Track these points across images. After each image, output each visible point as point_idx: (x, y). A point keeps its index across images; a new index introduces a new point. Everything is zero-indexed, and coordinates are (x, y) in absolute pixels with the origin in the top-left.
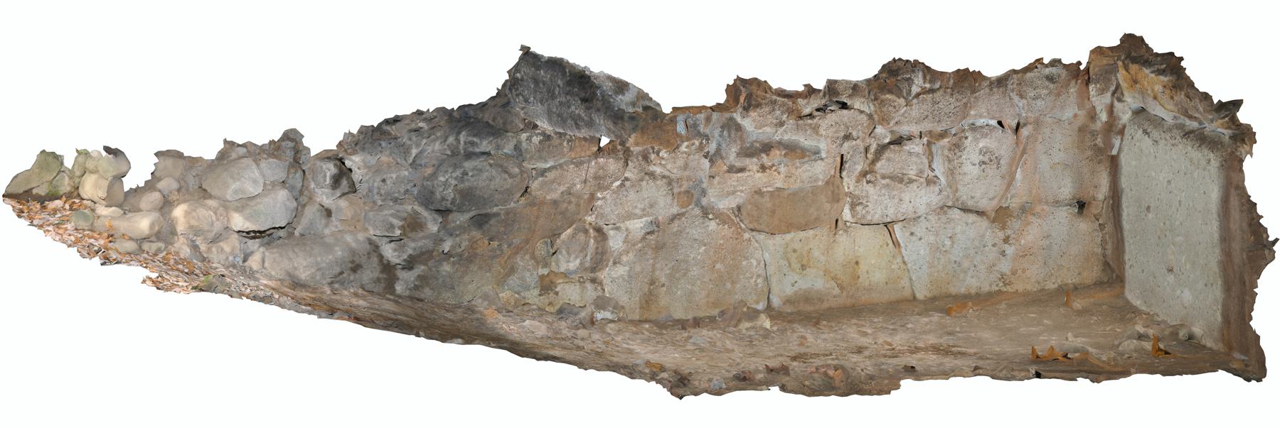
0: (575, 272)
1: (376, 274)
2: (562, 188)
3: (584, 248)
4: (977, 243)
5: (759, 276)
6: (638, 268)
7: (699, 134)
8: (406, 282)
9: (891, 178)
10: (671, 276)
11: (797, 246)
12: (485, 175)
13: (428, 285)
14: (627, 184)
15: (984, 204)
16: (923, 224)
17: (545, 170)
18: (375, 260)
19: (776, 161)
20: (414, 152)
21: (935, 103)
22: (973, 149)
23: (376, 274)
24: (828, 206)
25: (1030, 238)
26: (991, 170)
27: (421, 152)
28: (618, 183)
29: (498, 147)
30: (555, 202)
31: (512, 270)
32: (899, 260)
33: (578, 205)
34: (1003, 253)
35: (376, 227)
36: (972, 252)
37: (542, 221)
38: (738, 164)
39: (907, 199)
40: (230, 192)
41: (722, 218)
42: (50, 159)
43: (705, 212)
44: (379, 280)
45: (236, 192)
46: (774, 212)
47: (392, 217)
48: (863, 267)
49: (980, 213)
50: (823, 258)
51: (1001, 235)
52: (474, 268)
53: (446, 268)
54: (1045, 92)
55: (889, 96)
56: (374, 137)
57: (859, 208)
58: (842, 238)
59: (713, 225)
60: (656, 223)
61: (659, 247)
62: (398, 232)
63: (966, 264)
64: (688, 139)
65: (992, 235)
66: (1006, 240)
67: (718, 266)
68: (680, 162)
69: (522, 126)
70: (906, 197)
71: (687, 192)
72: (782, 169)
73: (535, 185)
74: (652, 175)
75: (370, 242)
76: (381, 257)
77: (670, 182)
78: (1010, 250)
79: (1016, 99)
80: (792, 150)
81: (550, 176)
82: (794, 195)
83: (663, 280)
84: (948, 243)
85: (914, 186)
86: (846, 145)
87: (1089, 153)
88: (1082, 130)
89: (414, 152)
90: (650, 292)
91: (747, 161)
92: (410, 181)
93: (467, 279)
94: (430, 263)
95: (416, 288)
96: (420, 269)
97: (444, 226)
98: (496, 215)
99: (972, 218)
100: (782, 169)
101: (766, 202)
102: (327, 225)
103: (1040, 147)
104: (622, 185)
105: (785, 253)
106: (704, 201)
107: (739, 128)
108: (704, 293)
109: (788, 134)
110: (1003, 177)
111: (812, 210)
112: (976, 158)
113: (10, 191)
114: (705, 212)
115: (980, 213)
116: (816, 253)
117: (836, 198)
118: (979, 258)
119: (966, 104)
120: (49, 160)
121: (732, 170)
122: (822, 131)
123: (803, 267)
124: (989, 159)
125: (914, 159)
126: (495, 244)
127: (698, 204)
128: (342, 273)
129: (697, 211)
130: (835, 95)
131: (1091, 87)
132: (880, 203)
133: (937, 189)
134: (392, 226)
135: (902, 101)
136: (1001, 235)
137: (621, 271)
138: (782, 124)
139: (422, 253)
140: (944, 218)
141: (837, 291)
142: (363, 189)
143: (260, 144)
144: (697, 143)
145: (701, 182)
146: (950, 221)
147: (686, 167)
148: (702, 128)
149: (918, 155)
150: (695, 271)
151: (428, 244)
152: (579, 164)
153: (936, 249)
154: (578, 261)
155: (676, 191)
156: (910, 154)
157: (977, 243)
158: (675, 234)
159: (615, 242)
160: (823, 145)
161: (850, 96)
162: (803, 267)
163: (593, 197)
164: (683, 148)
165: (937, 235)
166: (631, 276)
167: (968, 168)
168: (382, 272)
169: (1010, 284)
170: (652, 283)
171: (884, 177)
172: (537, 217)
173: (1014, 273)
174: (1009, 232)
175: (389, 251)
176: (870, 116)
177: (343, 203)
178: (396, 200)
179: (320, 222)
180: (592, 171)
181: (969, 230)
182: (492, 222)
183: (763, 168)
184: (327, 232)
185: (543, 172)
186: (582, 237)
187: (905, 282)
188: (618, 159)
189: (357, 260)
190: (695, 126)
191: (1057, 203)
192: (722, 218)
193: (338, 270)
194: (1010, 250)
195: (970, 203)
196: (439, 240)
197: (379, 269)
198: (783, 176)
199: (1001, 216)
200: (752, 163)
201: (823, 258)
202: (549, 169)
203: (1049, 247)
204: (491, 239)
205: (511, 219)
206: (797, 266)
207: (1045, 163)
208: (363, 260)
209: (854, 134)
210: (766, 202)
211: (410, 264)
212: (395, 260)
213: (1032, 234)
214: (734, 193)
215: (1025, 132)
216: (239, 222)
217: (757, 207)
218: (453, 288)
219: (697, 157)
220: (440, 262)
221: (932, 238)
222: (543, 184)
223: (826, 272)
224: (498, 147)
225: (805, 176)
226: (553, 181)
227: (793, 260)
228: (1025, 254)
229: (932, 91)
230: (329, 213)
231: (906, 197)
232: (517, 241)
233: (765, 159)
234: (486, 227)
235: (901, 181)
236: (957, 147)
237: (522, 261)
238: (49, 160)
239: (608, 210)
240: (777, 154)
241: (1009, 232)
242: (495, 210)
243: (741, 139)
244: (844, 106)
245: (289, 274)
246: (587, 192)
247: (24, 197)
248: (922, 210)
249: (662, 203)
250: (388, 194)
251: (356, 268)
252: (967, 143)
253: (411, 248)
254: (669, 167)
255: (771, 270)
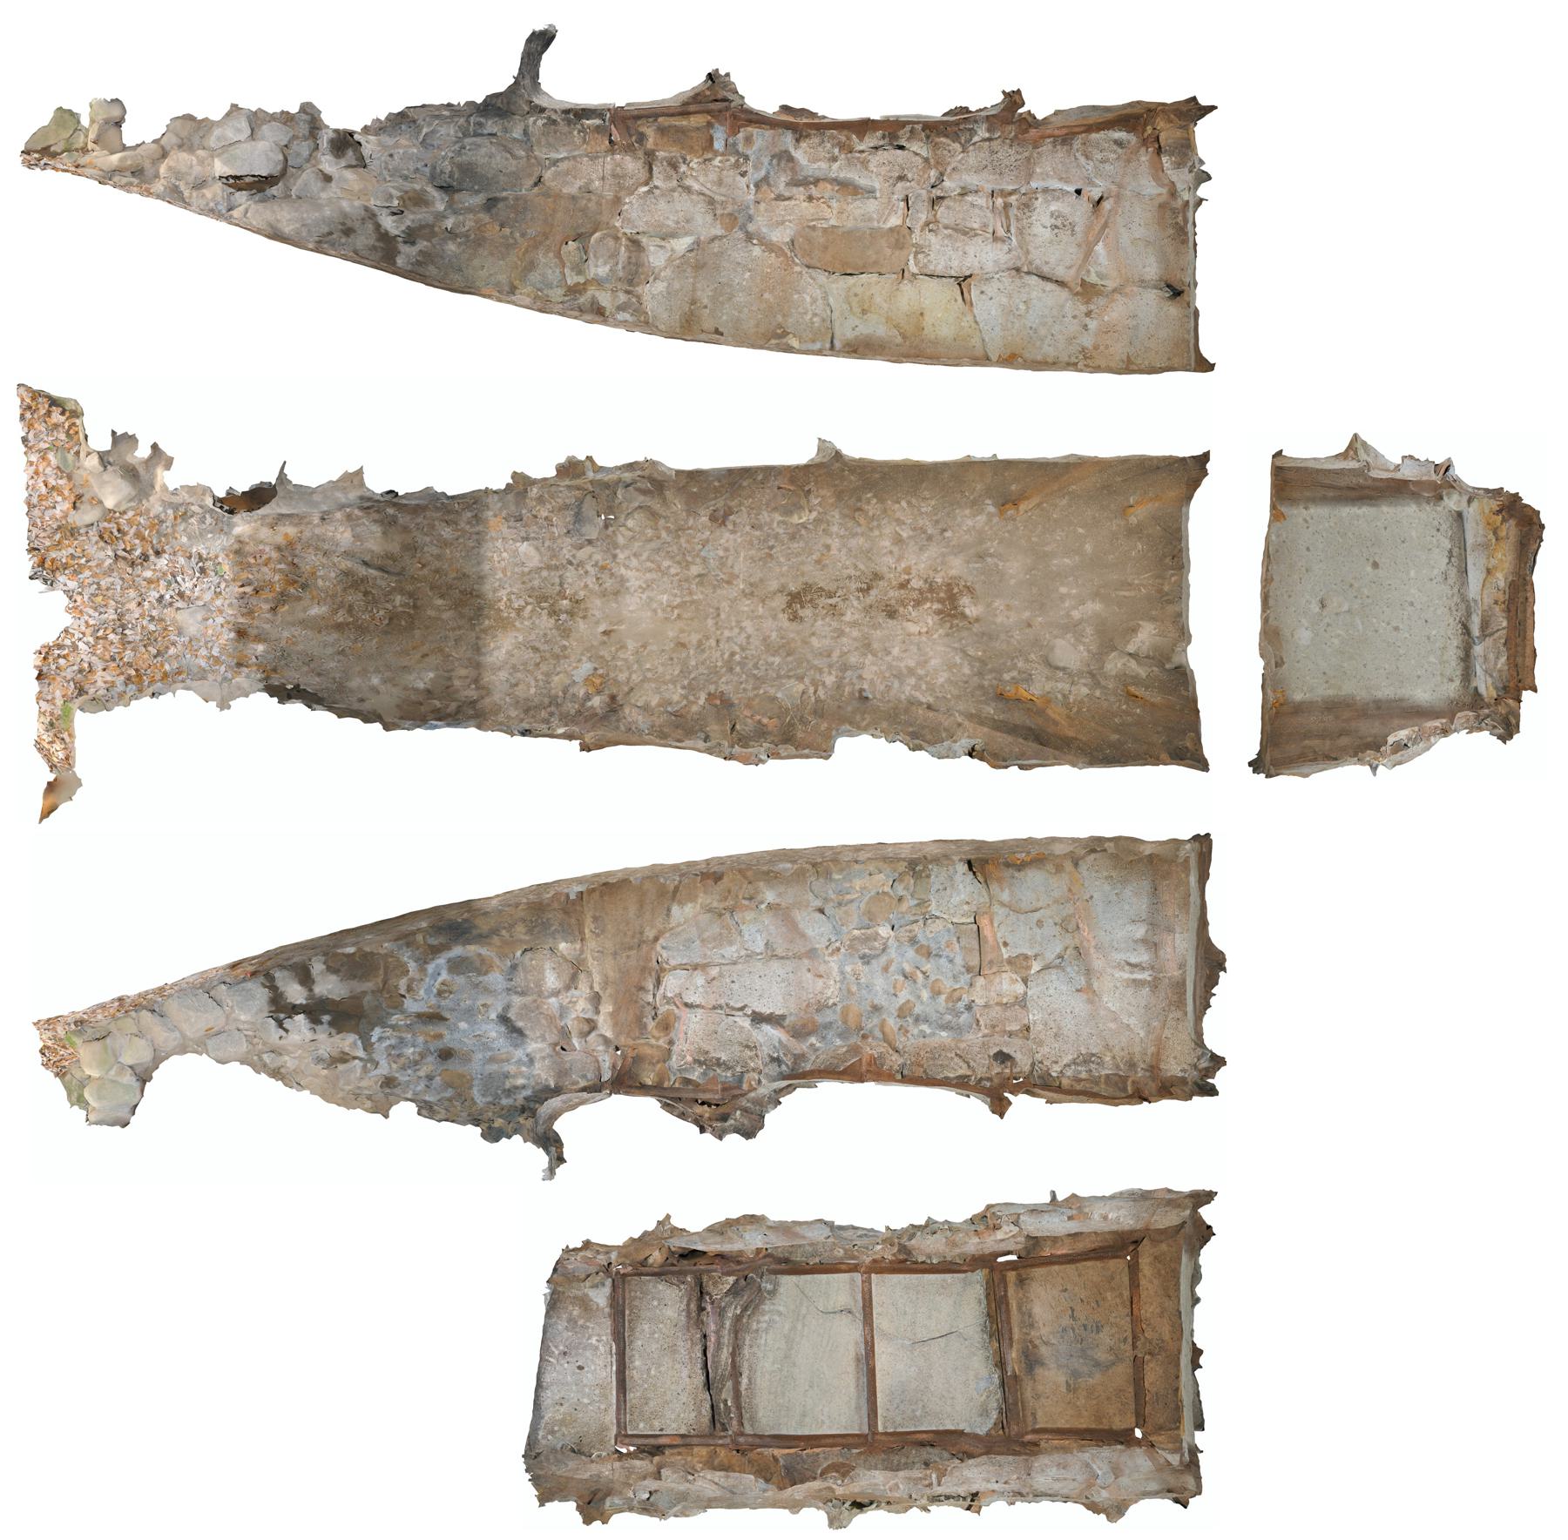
0: (607, 280)
1: (372, 242)
2: (579, 183)
3: (614, 255)
4: (1055, 312)
5: (815, 315)
6: (677, 286)
7: (737, 153)
8: (408, 256)
9: (955, 230)
10: (714, 299)
11: (859, 290)
12: (483, 151)
13: (433, 262)
14: (657, 192)
15: (1060, 272)
16: (995, 285)
17: (558, 160)
18: (370, 226)
19: (827, 195)
20: (425, 130)
21: (993, 152)
22: (1043, 214)
23: (372, 242)
24: (888, 251)
25: (1114, 315)
26: (1065, 236)
27: (433, 132)
28: (645, 189)
29: (506, 130)
30: (573, 198)
31: (532, 266)
32: (970, 318)
33: (599, 204)
34: (1085, 327)
35: (377, 198)
36: (1050, 320)
37: (560, 215)
38: (787, 194)
39: (972, 253)
40: (213, 138)
41: (770, 247)
42: (67, 116)
43: (749, 237)
44: (374, 248)
45: (218, 139)
46: (826, 248)
47: (394, 188)
48: (928, 321)
49: (1060, 283)
50: (885, 305)
51: (1083, 308)
52: (484, 252)
53: (451, 247)
54: (1113, 156)
55: (943, 140)
56: (403, 120)
57: (920, 256)
58: (906, 287)
59: (757, 251)
60: (698, 243)
61: (699, 267)
62: (396, 203)
63: (1043, 331)
64: (723, 154)
65: (1074, 307)
66: (1088, 314)
67: (766, 296)
68: (713, 176)
69: (527, 108)
70: (971, 250)
71: (730, 215)
72: (834, 204)
73: (548, 175)
74: (688, 190)
75: (367, 209)
76: (378, 226)
77: (711, 202)
78: (1093, 325)
79: (1082, 160)
80: (848, 188)
81: (563, 166)
82: (849, 234)
83: (705, 301)
84: (1022, 307)
85: (979, 239)
86: (900, 185)
87: (1171, 231)
88: (1162, 206)
89: (425, 130)
90: (691, 312)
91: (795, 190)
92: (419, 159)
93: (476, 262)
94: (434, 241)
95: (419, 263)
96: (422, 245)
97: (450, 205)
98: (505, 199)
99: (1050, 286)
100: (834, 204)
101: (819, 238)
102: (323, 189)
103: (1119, 219)
104: (650, 192)
105: (847, 297)
106: (751, 228)
107: (791, 159)
108: (752, 322)
109: (839, 170)
110: (1079, 245)
111: (870, 252)
112: (1049, 221)
113: (31, 147)
114: (749, 237)
115: (1060, 283)
116: (878, 299)
117: (899, 245)
118: (1057, 327)
119: (1028, 159)
120: (65, 117)
121: (780, 198)
122: (872, 166)
123: (864, 312)
124: (1061, 225)
125: (977, 211)
126: (507, 231)
127: (743, 228)
128: (330, 233)
129: (741, 235)
130: (892, 130)
131: (1164, 159)
132: (944, 254)
133: (1006, 248)
134: (391, 197)
135: (957, 146)
136: (1083, 308)
137: (660, 287)
138: (835, 159)
139: (422, 227)
140: (1018, 282)
141: (899, 340)
142: (374, 166)
143: (271, 111)
144: (733, 160)
145: (748, 207)
146: (1024, 285)
147: (720, 183)
148: (741, 148)
149: (981, 208)
150: (741, 298)
151: (430, 219)
152: (593, 158)
153: (1009, 312)
154: (607, 268)
155: (719, 212)
156: (973, 205)
157: (1055, 312)
158: (716, 255)
159: (656, 257)
160: (877, 186)
161: (908, 140)
162: (864, 312)
163: (617, 201)
164: (716, 162)
165: (1010, 297)
166: (669, 293)
167: (1037, 229)
168: (378, 240)
169: (1091, 358)
170: (693, 302)
171: (946, 227)
172: (554, 211)
173: (1096, 347)
174: (1092, 307)
175: (388, 223)
176: (926, 160)
177: (349, 175)
178: (406, 178)
179: (316, 185)
180: (608, 167)
181: (1045, 298)
182: (501, 205)
183: (810, 198)
184: (324, 195)
185: (555, 162)
186: (611, 243)
187: (976, 341)
188: (636, 158)
189: (349, 223)
190: (734, 144)
191: (1142, 283)
192: (770, 247)
193: (326, 230)
194: (1093, 325)
195: (1046, 270)
196: (441, 216)
197: (374, 236)
198: (834, 213)
199: (1087, 291)
200: (799, 192)
201: (885, 305)
202: (562, 160)
203: (1136, 327)
204: (502, 226)
205: (521, 207)
206: (857, 310)
207: (1125, 239)
208: (357, 225)
209: (910, 176)
210: (819, 238)
211: (411, 237)
212: (394, 232)
213: (1116, 311)
214: (783, 223)
215: (1106, 205)
216: (220, 168)
217: (809, 241)
218: (460, 270)
219: (731, 173)
220: (444, 240)
221: (1004, 300)
222: (557, 174)
223: (888, 319)
224: (506, 130)
225: (857, 212)
226: (567, 173)
227: (854, 304)
228: (1107, 330)
229: (989, 140)
230: (328, 179)
231: (971, 250)
232: (531, 232)
233: (814, 191)
234: (494, 211)
235: (965, 234)
236: (1027, 206)
237: (544, 259)
238: (65, 117)
239: (634, 215)
240: (827, 189)
241: (1092, 307)
242: (504, 194)
243: (793, 169)
244: (901, 148)
245: (271, 226)
246: (609, 195)
247: (40, 153)
248: (990, 267)
249: (699, 219)
250: (396, 170)
251: (348, 232)
252: (1037, 203)
253: (410, 219)
254: (702, 179)
255: (836, 315)
